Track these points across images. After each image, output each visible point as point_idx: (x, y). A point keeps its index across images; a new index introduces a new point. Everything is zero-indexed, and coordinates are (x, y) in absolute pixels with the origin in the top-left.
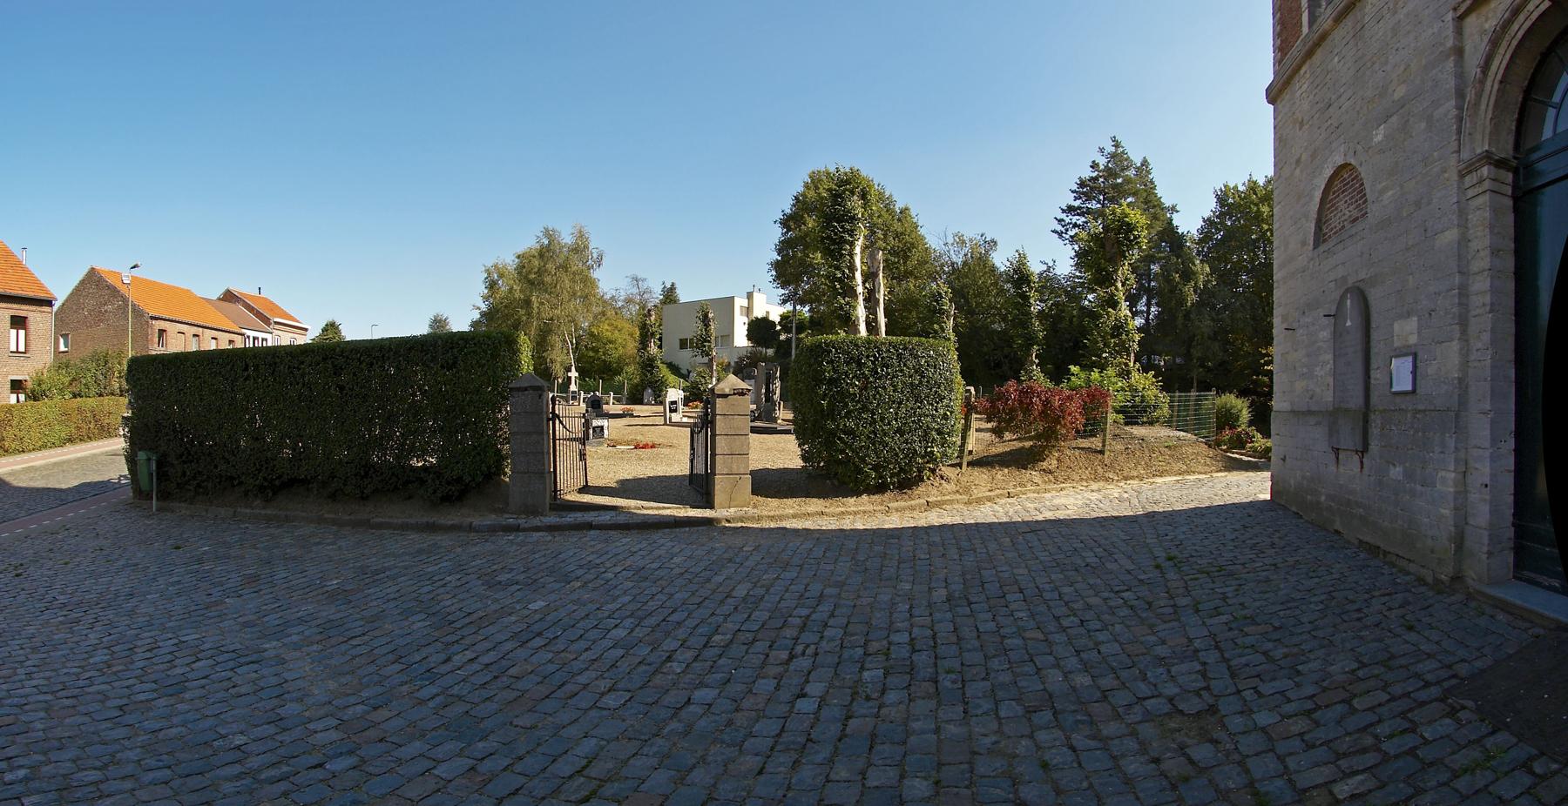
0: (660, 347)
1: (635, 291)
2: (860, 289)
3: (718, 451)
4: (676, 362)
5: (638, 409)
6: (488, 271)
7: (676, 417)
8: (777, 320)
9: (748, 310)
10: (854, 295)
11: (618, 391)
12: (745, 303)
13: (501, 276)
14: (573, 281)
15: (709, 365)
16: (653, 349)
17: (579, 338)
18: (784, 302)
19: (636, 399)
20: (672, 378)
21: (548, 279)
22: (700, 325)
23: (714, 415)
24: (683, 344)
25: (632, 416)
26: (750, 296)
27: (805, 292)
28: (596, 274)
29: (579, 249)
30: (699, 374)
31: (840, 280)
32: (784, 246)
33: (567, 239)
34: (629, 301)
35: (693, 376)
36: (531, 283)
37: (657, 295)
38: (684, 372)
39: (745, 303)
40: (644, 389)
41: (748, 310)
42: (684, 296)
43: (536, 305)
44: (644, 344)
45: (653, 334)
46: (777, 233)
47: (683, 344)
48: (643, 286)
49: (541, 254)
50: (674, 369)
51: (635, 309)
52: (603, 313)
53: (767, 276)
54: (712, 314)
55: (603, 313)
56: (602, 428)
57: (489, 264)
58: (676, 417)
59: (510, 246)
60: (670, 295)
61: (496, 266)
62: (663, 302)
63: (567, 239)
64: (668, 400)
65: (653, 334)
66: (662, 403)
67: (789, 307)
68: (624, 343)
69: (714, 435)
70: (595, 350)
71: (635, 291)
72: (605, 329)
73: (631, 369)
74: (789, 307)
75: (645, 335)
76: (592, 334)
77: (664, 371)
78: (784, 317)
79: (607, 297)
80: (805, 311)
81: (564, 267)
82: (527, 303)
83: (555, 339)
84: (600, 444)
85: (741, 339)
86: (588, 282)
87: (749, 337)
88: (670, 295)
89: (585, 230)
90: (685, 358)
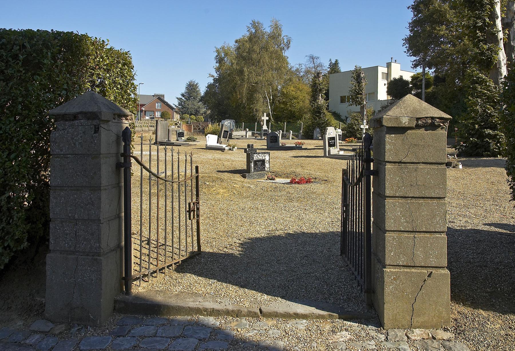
0: (327, 99)
1: (312, 65)
2: (501, 35)
3: (389, 224)
4: (338, 111)
5: (308, 143)
6: (217, 51)
7: (334, 151)
8: (410, 80)
9: (388, 75)
10: (496, 41)
11: (296, 130)
12: (385, 70)
13: (226, 54)
14: (271, 58)
15: (362, 112)
16: (321, 101)
17: (274, 96)
18: (415, 66)
19: (309, 136)
20: (334, 121)
21: (254, 56)
22: (355, 83)
23: (381, 162)
24: (343, 100)
25: (300, 148)
26: (389, 66)
27: (433, 58)
28: (286, 53)
29: (275, 36)
30: (354, 118)
31: (481, 29)
32: (414, 24)
33: (267, 29)
34: (307, 72)
35: (349, 121)
36: (244, 59)
37: (326, 68)
38: (343, 118)
39: (385, 70)
40: (314, 128)
41: (388, 75)
42: (344, 67)
43: (246, 74)
44: (314, 97)
45: (320, 90)
46: (410, 16)
47: (343, 100)
48: (317, 62)
49: (250, 39)
50: (337, 116)
51: (311, 77)
52: (290, 80)
53: (401, 49)
54: (362, 79)
55: (290, 80)
56: (263, 162)
57: (219, 47)
58: (334, 151)
59: (231, 36)
60: (334, 67)
61: (223, 48)
62: (330, 73)
63: (267, 29)
64: (327, 136)
65: (320, 90)
66: (323, 139)
67: (419, 70)
68: (302, 98)
69: (381, 196)
70: (285, 103)
71: (312, 65)
72: (291, 89)
73: (308, 116)
74: (419, 70)
75: (315, 90)
76: (283, 94)
77: (329, 116)
78: (414, 78)
79: (294, 69)
80: (431, 72)
81: (265, 48)
82: (241, 72)
83: (259, 96)
84: (261, 176)
85: (383, 95)
86: (282, 60)
87: (389, 93)
88: (334, 67)
89: (279, 23)
90: (344, 109)
